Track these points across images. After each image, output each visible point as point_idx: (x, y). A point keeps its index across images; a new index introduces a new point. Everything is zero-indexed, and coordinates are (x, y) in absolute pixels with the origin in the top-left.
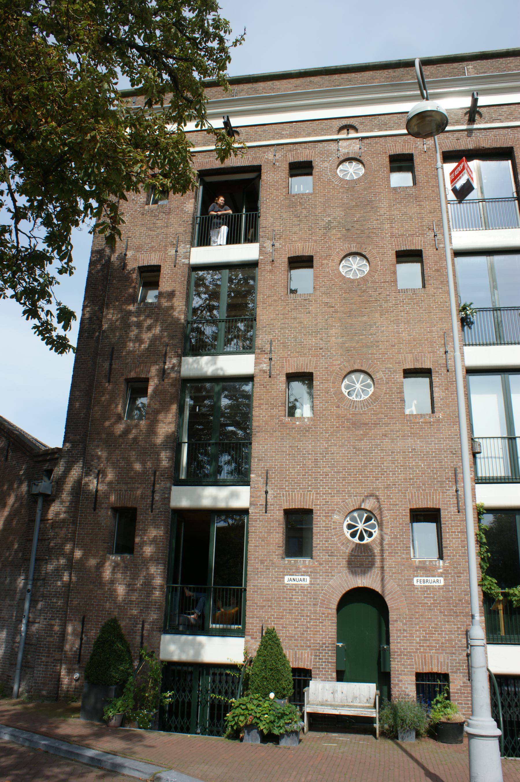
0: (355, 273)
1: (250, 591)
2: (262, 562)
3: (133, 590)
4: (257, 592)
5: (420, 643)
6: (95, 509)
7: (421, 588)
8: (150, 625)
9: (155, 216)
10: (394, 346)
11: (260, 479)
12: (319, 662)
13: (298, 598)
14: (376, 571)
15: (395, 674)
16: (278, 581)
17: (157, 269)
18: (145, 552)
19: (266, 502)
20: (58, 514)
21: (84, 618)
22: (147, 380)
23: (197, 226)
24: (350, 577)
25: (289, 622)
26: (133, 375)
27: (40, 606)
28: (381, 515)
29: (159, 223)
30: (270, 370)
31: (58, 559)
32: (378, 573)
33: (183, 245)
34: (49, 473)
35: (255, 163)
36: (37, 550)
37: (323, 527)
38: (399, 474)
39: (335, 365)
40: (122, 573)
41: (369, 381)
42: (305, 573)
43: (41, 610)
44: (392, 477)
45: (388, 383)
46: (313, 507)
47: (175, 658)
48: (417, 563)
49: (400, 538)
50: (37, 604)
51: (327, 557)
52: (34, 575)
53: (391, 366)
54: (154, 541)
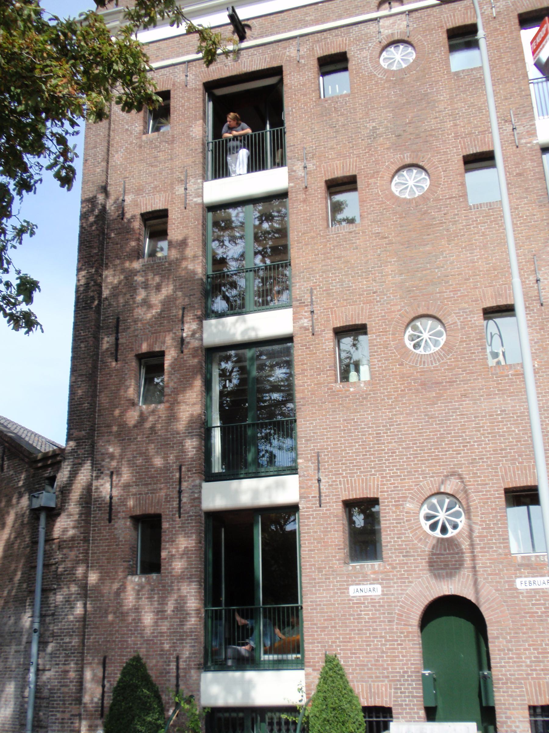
0: (412, 190)
1: (307, 609)
2: (320, 570)
3: (162, 619)
4: (316, 609)
5: (531, 666)
6: (110, 520)
7: (527, 592)
8: (185, 661)
9: (156, 147)
10: (468, 279)
11: (310, 464)
12: (401, 697)
13: (368, 614)
14: (466, 572)
15: (501, 709)
16: (341, 593)
17: (163, 214)
18: (173, 569)
19: (320, 493)
20: (65, 530)
21: (105, 658)
22: (162, 354)
23: (210, 154)
24: (433, 581)
25: (360, 645)
26: (144, 348)
27: (50, 648)
28: (467, 500)
29: (162, 156)
30: (312, 326)
31: (69, 588)
32: (468, 576)
33: (193, 180)
34: (52, 480)
35: (275, 64)
36: (43, 579)
37: (393, 519)
38: (486, 444)
39: (394, 312)
40: (148, 598)
41: (439, 328)
42: (375, 581)
43: (51, 654)
44: (478, 449)
45: (464, 328)
46: (379, 495)
47: (221, 702)
48: (519, 560)
49: (493, 528)
50: (46, 647)
51: (402, 558)
52: (41, 611)
53: (466, 306)
54: (186, 553)
